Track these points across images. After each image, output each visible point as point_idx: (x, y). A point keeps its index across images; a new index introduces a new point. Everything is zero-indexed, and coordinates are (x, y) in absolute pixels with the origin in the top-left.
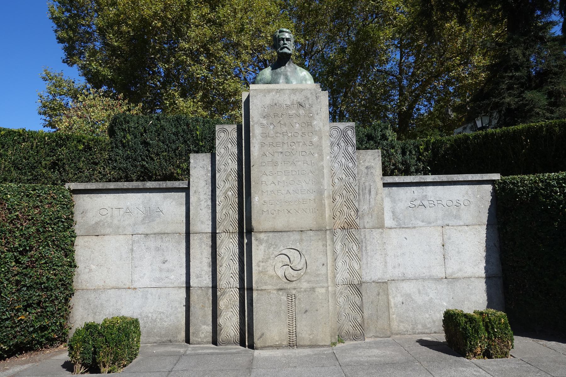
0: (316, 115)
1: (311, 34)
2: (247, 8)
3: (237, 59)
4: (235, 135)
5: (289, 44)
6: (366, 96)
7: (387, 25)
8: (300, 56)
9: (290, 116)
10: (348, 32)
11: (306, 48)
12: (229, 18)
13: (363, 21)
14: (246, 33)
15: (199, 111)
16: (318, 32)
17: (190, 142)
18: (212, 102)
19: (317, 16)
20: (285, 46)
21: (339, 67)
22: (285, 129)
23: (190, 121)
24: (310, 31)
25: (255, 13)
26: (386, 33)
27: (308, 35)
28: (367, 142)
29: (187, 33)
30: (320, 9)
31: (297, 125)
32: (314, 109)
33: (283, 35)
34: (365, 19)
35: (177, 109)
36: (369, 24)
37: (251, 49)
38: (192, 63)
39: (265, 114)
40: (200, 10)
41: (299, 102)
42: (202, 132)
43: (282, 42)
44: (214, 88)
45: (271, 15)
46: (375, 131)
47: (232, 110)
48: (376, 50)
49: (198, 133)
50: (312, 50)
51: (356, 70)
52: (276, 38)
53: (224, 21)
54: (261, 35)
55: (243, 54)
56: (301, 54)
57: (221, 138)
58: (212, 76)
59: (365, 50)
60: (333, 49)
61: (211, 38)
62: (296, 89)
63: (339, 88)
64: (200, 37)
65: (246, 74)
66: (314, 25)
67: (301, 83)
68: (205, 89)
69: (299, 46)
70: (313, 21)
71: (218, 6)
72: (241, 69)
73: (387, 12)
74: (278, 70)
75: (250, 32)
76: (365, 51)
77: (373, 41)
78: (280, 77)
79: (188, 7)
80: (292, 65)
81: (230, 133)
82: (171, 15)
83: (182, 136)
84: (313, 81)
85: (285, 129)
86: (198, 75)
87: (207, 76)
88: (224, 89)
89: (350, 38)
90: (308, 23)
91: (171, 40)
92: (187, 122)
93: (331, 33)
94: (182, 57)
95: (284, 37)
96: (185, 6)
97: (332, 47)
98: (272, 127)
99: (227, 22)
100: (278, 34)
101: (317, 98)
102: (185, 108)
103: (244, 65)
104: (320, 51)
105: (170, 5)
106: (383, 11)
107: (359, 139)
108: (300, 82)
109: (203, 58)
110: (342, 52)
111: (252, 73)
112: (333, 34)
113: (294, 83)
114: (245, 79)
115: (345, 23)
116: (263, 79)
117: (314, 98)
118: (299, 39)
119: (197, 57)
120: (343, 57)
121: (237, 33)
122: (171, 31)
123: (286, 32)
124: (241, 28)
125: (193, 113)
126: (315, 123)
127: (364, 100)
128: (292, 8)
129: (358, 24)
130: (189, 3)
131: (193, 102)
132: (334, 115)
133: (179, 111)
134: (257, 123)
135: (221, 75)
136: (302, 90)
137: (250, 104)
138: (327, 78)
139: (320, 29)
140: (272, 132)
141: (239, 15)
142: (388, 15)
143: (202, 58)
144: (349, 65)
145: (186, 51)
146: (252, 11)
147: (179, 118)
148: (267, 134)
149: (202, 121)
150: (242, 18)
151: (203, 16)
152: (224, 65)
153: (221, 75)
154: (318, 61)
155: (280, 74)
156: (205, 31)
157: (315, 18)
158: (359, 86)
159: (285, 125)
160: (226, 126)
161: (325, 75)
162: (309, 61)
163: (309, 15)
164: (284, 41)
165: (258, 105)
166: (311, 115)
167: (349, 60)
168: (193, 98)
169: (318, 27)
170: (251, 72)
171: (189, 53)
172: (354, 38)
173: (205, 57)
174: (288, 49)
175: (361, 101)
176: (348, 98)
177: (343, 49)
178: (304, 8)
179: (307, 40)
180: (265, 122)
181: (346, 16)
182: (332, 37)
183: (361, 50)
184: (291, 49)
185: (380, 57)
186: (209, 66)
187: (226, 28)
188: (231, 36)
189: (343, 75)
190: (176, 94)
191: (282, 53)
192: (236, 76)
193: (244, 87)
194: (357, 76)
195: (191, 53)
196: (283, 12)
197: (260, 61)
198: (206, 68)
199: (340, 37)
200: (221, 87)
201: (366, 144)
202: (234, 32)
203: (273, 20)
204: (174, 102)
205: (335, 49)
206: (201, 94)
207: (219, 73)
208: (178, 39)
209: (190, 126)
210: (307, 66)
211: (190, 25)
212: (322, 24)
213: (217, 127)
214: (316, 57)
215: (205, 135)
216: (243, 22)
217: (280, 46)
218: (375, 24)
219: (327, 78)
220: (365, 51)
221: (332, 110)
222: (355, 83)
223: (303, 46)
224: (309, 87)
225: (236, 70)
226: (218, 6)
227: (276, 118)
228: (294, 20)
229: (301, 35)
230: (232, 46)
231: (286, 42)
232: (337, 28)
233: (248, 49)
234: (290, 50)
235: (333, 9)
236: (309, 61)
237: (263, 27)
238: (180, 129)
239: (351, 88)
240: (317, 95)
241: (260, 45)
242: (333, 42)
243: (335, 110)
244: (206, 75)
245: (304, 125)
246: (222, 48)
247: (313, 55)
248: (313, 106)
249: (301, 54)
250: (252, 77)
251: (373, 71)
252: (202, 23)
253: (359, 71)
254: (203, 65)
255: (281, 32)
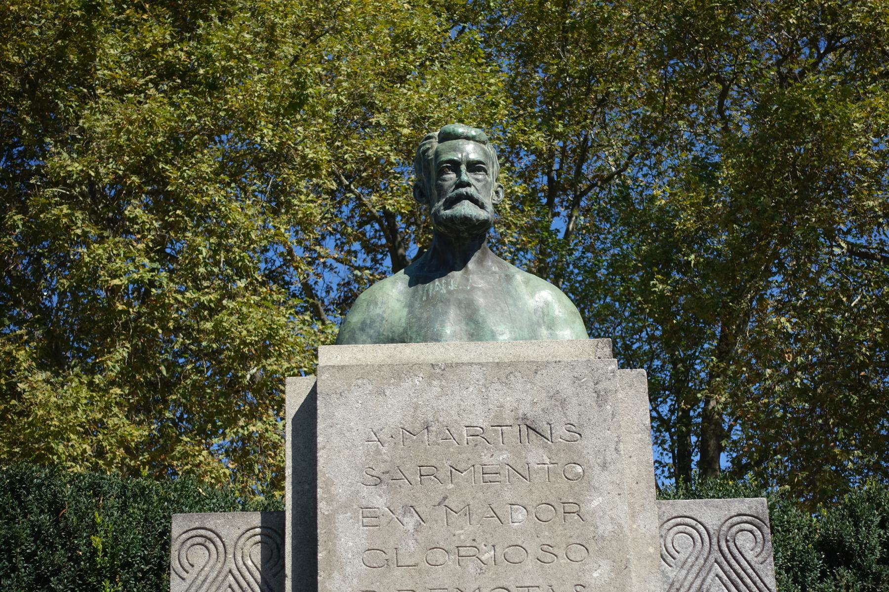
0: (597, 469)
1: (572, 115)
2: (318, 23)
3: (276, 212)
4: (254, 555)
5: (479, 185)
6: (812, 352)
7: (874, 79)
8: (531, 198)
9: (488, 476)
10: (721, 104)
11: (556, 166)
12: (246, 61)
13: (779, 63)
14: (315, 114)
15: (111, 422)
16: (601, 103)
17: (60, 581)
18: (168, 386)
19: (594, 44)
20: (463, 190)
21: (691, 240)
22: (465, 531)
23: (68, 489)
24: (569, 102)
25: (351, 40)
26: (875, 109)
27: (560, 118)
28: (823, 573)
29: (78, 118)
30: (605, 22)
31: (520, 515)
32: (588, 445)
33: (455, 149)
34: (787, 56)
35: (21, 414)
36: (802, 74)
37: (331, 174)
38: (93, 232)
39: (383, 467)
40: (136, 32)
41: (525, 418)
42: (115, 539)
43: (451, 176)
44: (178, 329)
45: (414, 46)
46: (856, 525)
47: (252, 416)
48: (841, 172)
49: (97, 541)
50: (578, 172)
51: (761, 250)
52: (428, 162)
53: (227, 70)
54: (374, 121)
55: (299, 192)
56: (535, 190)
57: (193, 572)
58: (171, 280)
59: (794, 173)
60: (662, 168)
61: (172, 135)
62: (511, 364)
63: (697, 321)
64: (128, 132)
65: (311, 271)
66: (587, 78)
67: (533, 336)
68: (140, 332)
69: (527, 160)
70: (579, 64)
71: (207, 19)
72: (290, 252)
73: (872, 29)
74: (438, 286)
75: (328, 108)
76: (795, 177)
77: (823, 138)
78: (446, 313)
79: (88, 22)
80: (493, 264)
81: (230, 550)
82: (19, 54)
83: (29, 558)
84: (579, 325)
85: (465, 531)
86: (114, 277)
87: (152, 283)
88: (220, 333)
89: (731, 126)
90: (561, 71)
91: (15, 145)
92: (55, 495)
93: (654, 109)
94: (55, 211)
95: (457, 156)
96: (75, 19)
97: (660, 162)
98: (410, 522)
99: (240, 76)
100: (435, 144)
101: (601, 397)
102: (54, 413)
103: (301, 235)
104: (611, 177)
105: (17, 18)
106: (854, 25)
107: (792, 559)
108: (526, 334)
109: (139, 212)
110: (702, 179)
111: (335, 264)
112: (662, 112)
113: (505, 335)
114: (308, 289)
115: (709, 70)
116: (373, 321)
117: (589, 399)
118: (524, 132)
119: (117, 203)
120: (707, 201)
121: (277, 114)
122: (15, 109)
123: (468, 138)
124: (292, 96)
125: (86, 432)
126: (595, 503)
127: (804, 368)
128: (498, 20)
129: (758, 76)
130: (92, 9)
131: (91, 384)
132: (679, 431)
133: (31, 424)
134: (346, 507)
135: (210, 275)
136: (537, 367)
137: (321, 426)
138: (645, 282)
139: (608, 94)
140: (411, 542)
141: (288, 50)
142: (877, 41)
143: (134, 210)
144: (732, 231)
145: (72, 186)
146: (336, 31)
147: (21, 481)
148: (391, 554)
149: (116, 490)
150: (296, 58)
151: (146, 54)
152: (222, 236)
153: (210, 275)
154: (604, 214)
155: (446, 302)
156: (150, 110)
157: (588, 54)
158: (778, 311)
159: (467, 511)
160: (216, 521)
161: (636, 269)
162: (570, 217)
163: (564, 41)
164: (458, 173)
165: (350, 430)
166: (579, 469)
167: (732, 213)
168: (91, 371)
169: (601, 87)
170: (330, 261)
171: (82, 193)
172: (745, 128)
173: (146, 206)
174: (475, 201)
175: (791, 375)
176: (736, 363)
177: (704, 167)
178: (542, 16)
179: (558, 136)
180: (379, 501)
181: (709, 46)
182: (659, 124)
183: (778, 171)
184: (488, 203)
185: (859, 199)
186: (161, 241)
187: (235, 99)
188: (254, 128)
189: (709, 268)
190: (21, 355)
191: (452, 219)
192: (272, 276)
193: (303, 322)
194: (768, 273)
195: (92, 193)
196: (462, 31)
197: (369, 218)
198: (148, 251)
199: (692, 124)
200: (209, 325)
201: (821, 579)
202: (266, 111)
203: (422, 65)
204: (12, 386)
205: (674, 168)
206: (122, 352)
207: (202, 270)
208: (41, 142)
209: (65, 512)
210: (561, 236)
211: (91, 88)
212: (615, 75)
213: (179, 525)
214: (597, 200)
215: (127, 551)
216: (300, 75)
217: (441, 191)
218: (828, 74)
219: (645, 282)
220: (795, 177)
221: (672, 411)
222: (761, 300)
223: (544, 159)
224: (563, 353)
225: (270, 254)
226: (207, 19)
227: (429, 482)
228: (505, 62)
229: (533, 116)
230: (258, 163)
231: (466, 177)
232: (676, 89)
233: (318, 176)
234: (482, 206)
235: (658, 20)
236: (570, 217)
237: (381, 89)
238: (22, 529)
239: (745, 323)
240: (601, 387)
241: (369, 157)
242: (662, 140)
243: (686, 413)
244: (148, 276)
245: (547, 513)
246: (216, 173)
247: (584, 193)
248: (587, 432)
249: (535, 190)
250: (333, 280)
251: (832, 253)
252: (141, 81)
253: (776, 254)
254: (138, 241)
255: (446, 137)
